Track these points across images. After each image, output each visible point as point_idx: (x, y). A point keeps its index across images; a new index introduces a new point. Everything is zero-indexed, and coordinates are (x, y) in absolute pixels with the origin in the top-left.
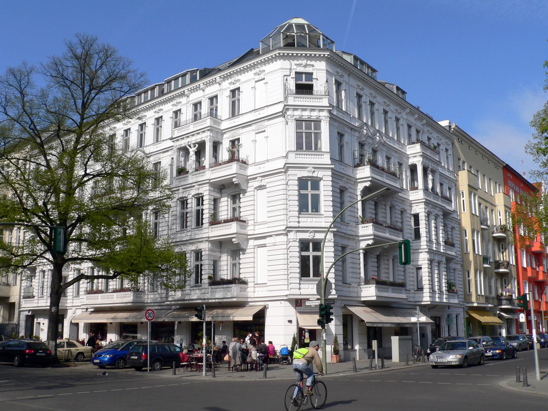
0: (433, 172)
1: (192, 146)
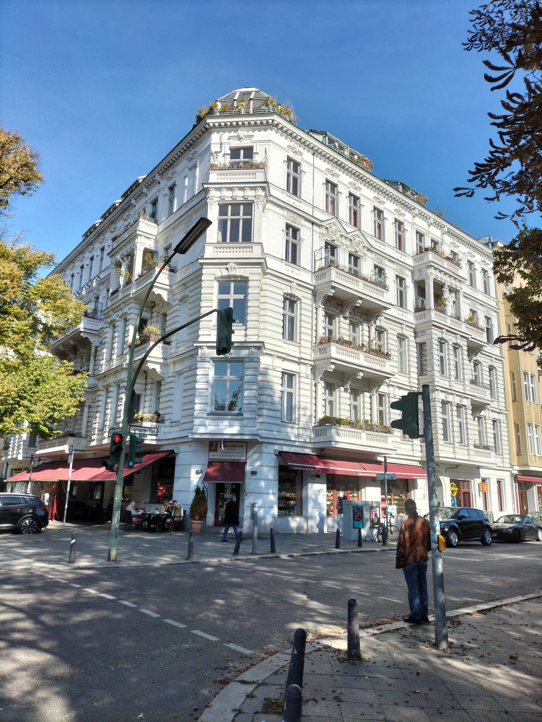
0: (452, 290)
1: (125, 259)
